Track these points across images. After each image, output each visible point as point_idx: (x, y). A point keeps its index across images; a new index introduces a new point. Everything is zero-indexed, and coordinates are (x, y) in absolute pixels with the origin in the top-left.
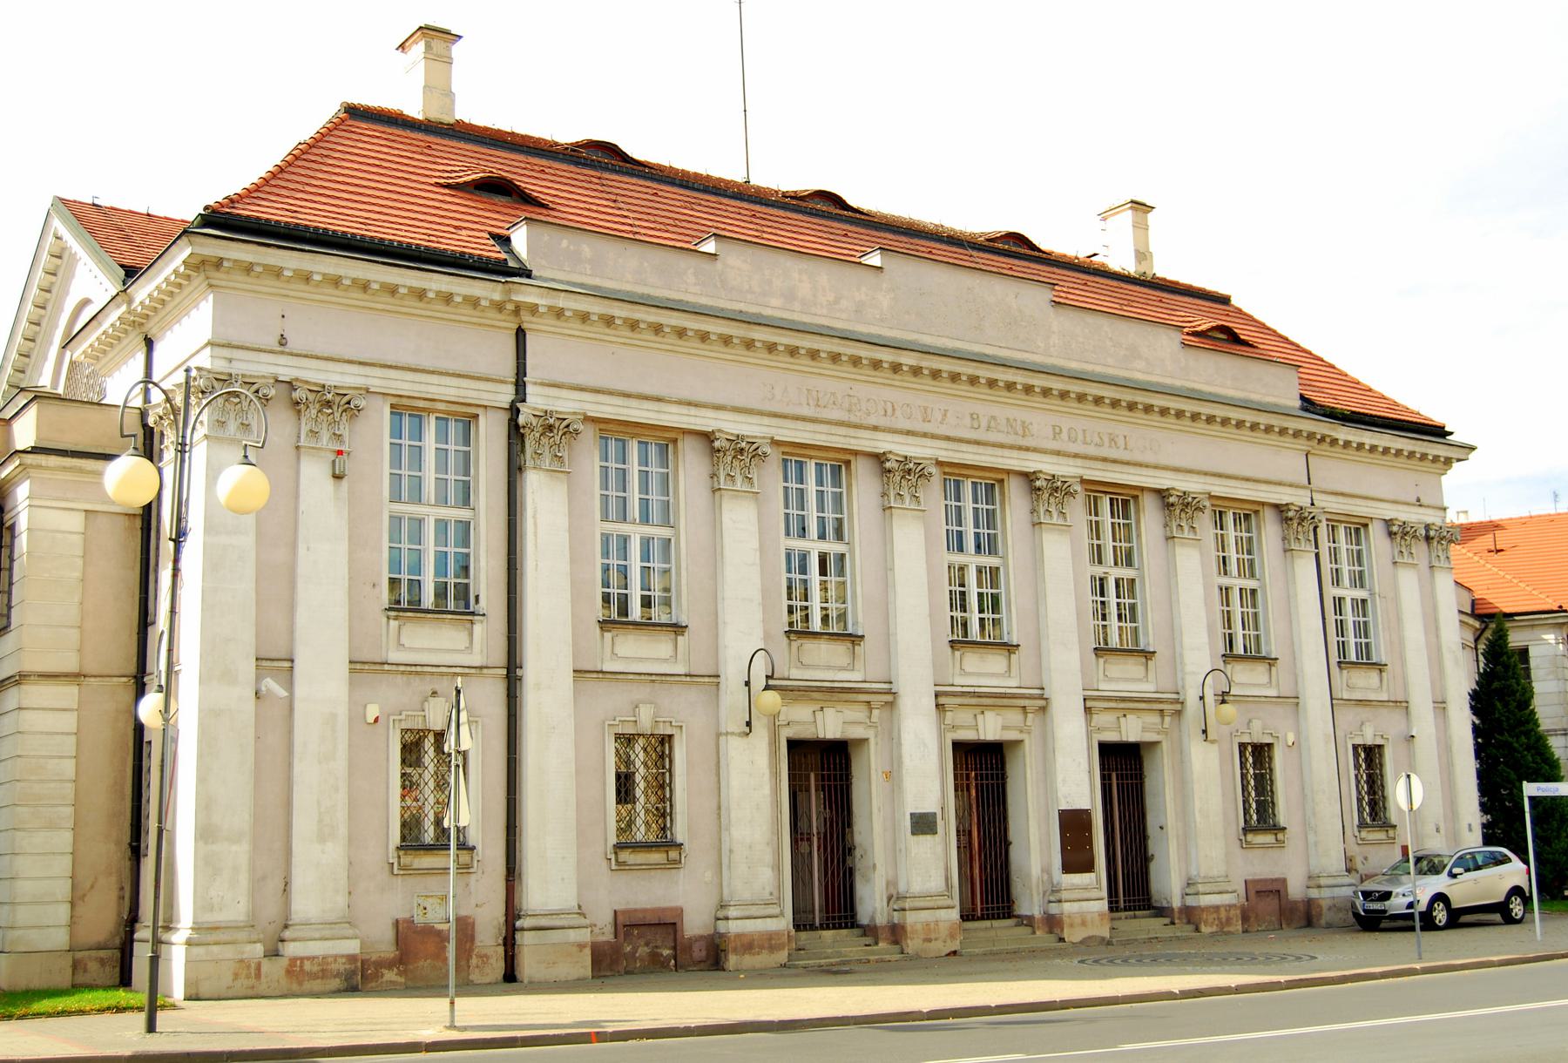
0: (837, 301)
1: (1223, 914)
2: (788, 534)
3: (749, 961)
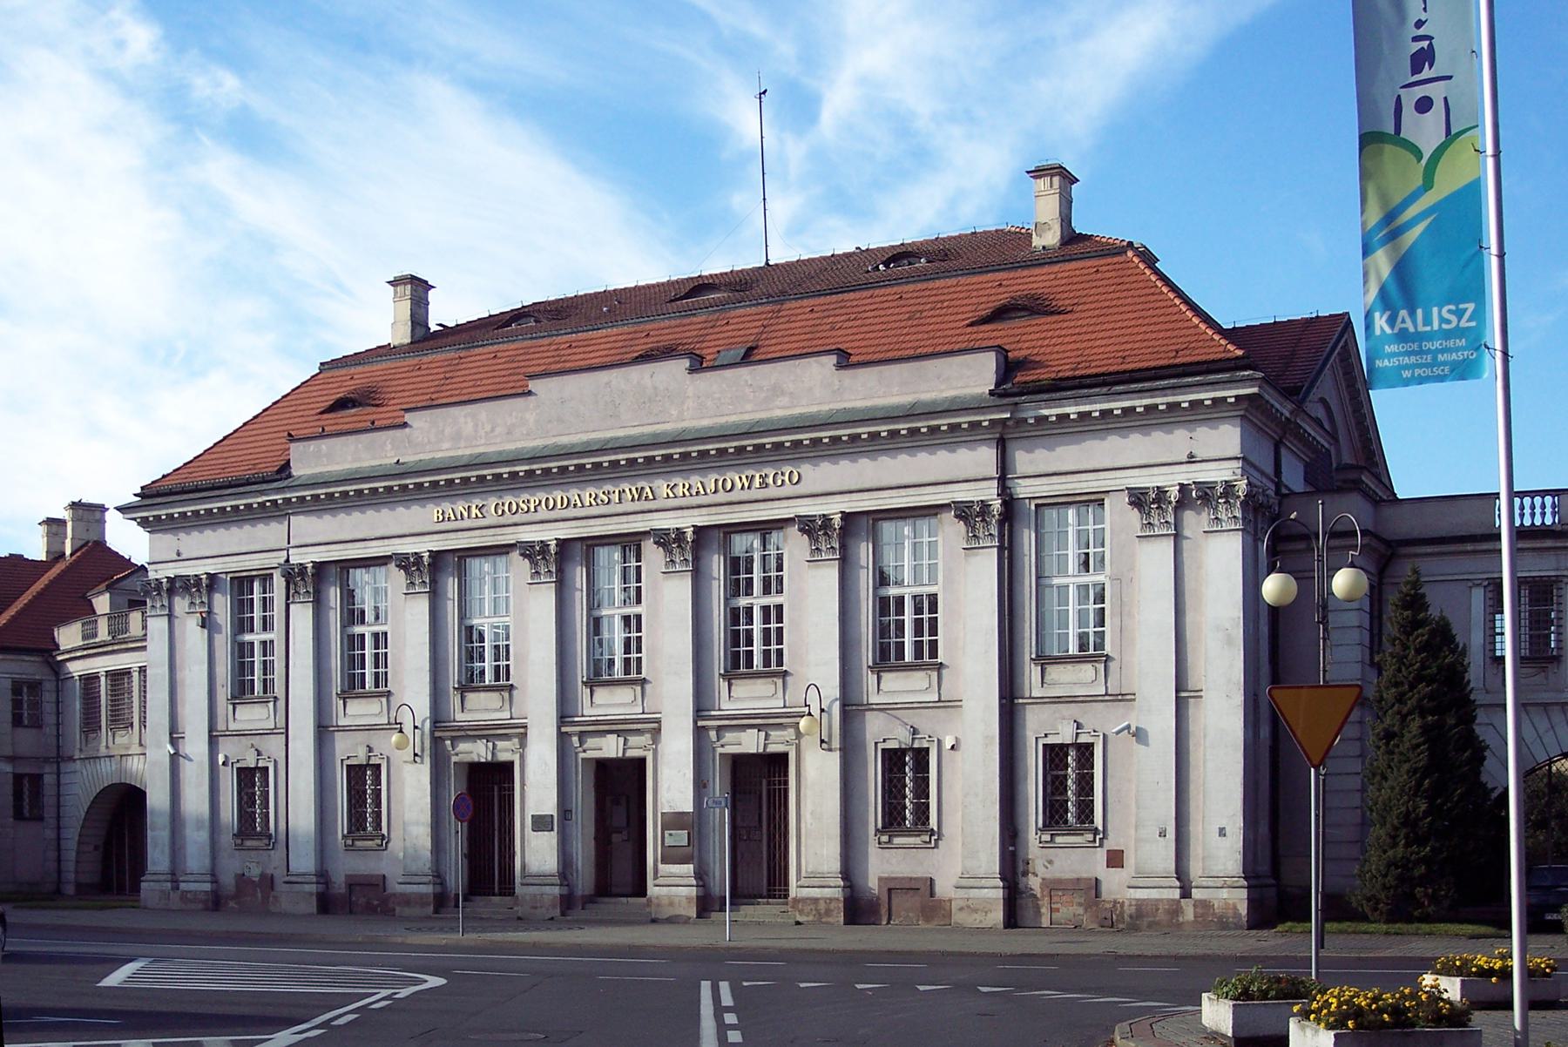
0: (493, 430)
1: (822, 906)
2: (144, 648)
3: (407, 911)
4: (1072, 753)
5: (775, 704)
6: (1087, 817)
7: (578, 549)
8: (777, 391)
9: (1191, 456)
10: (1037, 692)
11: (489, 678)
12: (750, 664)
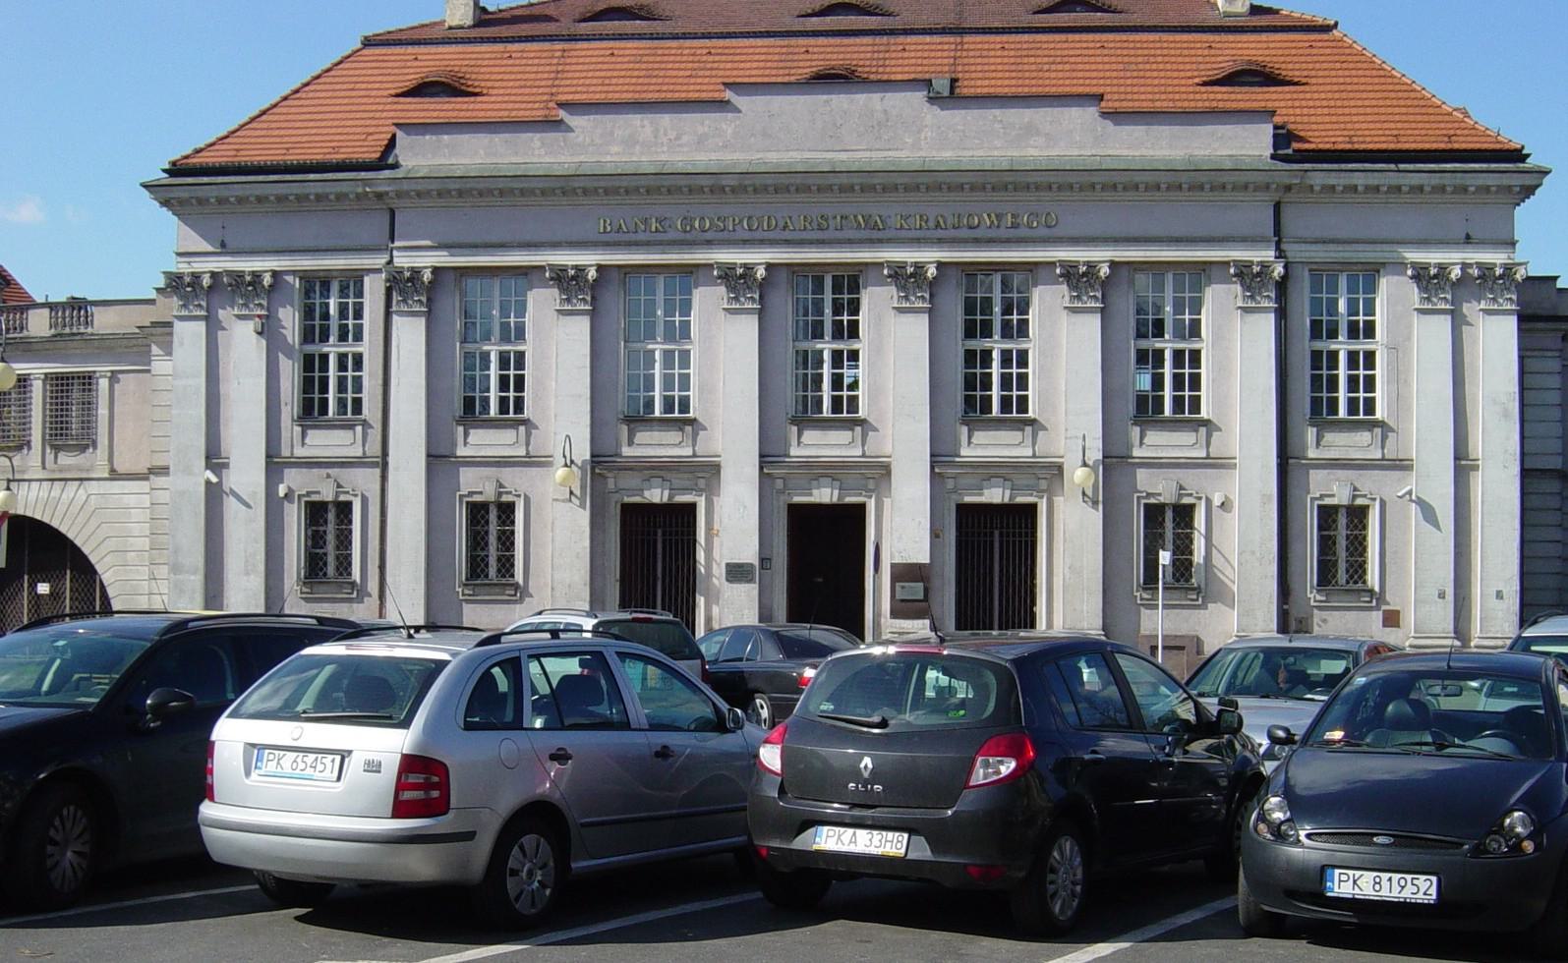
0: (678, 138)
4: (1169, 515)
5: (1024, 452)
6: (508, 571)
7: (783, 275)
8: (1030, 130)
9: (1468, 237)
10: (1312, 453)
11: (493, 411)
12: (324, 410)
